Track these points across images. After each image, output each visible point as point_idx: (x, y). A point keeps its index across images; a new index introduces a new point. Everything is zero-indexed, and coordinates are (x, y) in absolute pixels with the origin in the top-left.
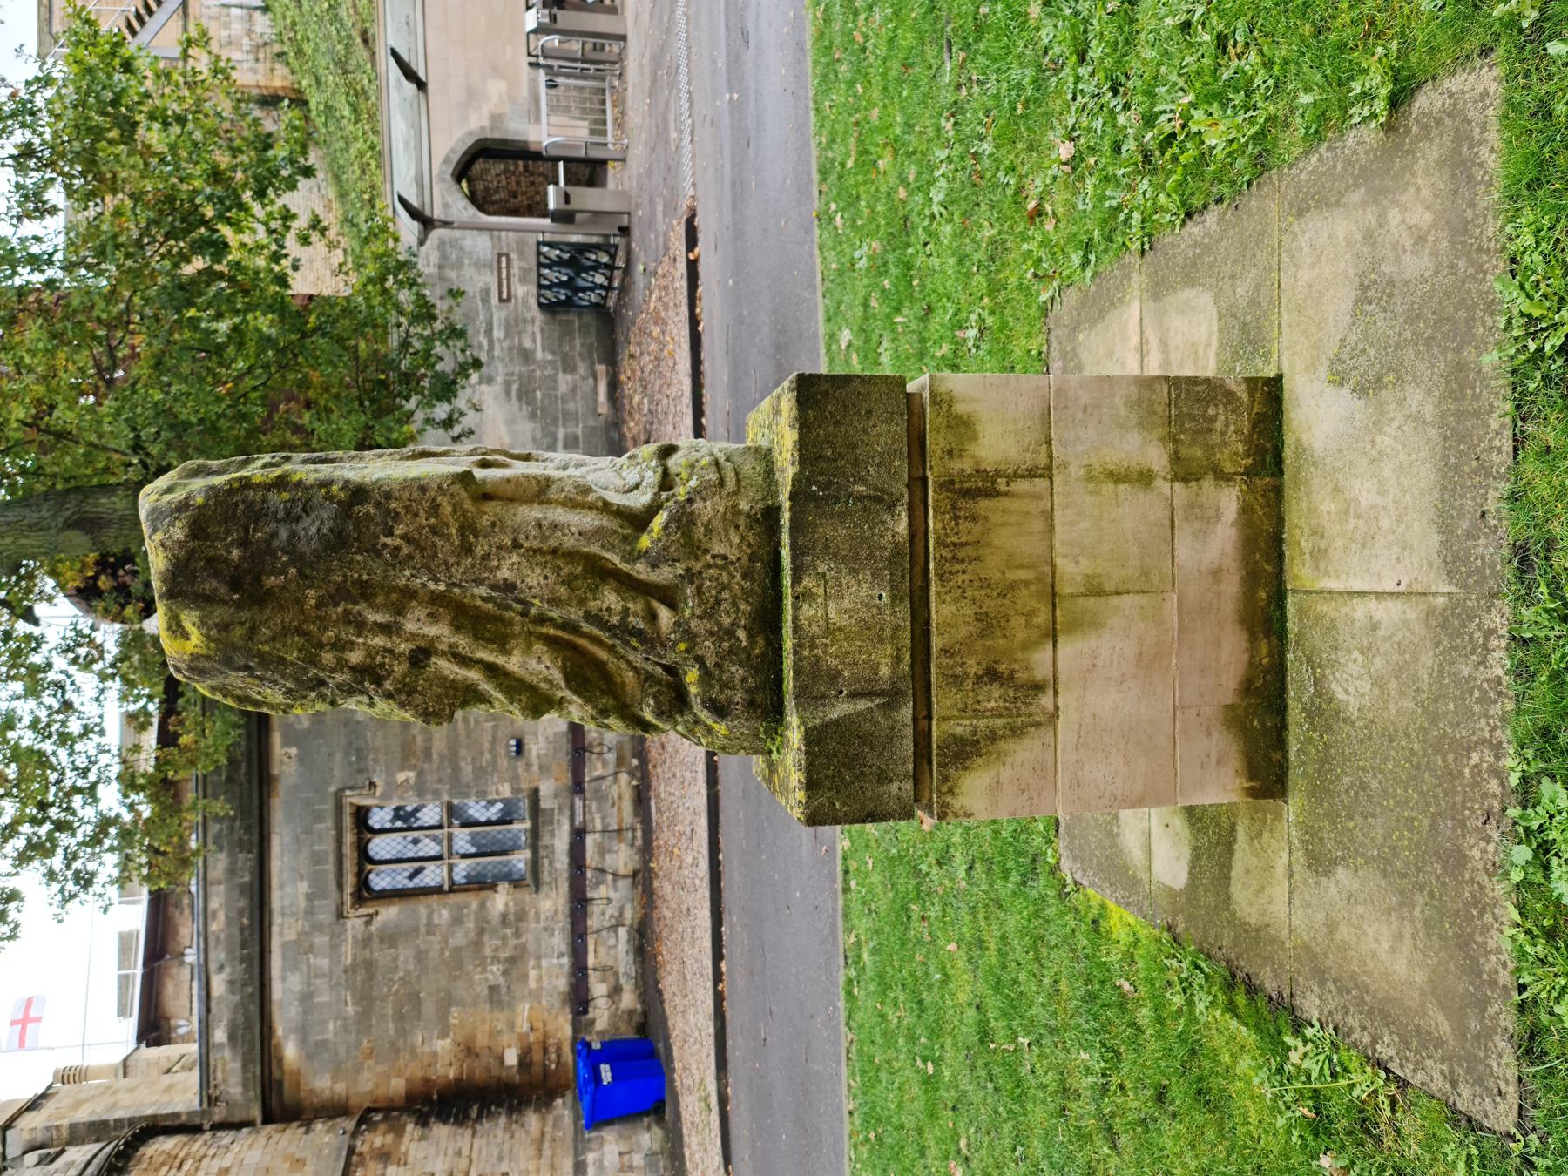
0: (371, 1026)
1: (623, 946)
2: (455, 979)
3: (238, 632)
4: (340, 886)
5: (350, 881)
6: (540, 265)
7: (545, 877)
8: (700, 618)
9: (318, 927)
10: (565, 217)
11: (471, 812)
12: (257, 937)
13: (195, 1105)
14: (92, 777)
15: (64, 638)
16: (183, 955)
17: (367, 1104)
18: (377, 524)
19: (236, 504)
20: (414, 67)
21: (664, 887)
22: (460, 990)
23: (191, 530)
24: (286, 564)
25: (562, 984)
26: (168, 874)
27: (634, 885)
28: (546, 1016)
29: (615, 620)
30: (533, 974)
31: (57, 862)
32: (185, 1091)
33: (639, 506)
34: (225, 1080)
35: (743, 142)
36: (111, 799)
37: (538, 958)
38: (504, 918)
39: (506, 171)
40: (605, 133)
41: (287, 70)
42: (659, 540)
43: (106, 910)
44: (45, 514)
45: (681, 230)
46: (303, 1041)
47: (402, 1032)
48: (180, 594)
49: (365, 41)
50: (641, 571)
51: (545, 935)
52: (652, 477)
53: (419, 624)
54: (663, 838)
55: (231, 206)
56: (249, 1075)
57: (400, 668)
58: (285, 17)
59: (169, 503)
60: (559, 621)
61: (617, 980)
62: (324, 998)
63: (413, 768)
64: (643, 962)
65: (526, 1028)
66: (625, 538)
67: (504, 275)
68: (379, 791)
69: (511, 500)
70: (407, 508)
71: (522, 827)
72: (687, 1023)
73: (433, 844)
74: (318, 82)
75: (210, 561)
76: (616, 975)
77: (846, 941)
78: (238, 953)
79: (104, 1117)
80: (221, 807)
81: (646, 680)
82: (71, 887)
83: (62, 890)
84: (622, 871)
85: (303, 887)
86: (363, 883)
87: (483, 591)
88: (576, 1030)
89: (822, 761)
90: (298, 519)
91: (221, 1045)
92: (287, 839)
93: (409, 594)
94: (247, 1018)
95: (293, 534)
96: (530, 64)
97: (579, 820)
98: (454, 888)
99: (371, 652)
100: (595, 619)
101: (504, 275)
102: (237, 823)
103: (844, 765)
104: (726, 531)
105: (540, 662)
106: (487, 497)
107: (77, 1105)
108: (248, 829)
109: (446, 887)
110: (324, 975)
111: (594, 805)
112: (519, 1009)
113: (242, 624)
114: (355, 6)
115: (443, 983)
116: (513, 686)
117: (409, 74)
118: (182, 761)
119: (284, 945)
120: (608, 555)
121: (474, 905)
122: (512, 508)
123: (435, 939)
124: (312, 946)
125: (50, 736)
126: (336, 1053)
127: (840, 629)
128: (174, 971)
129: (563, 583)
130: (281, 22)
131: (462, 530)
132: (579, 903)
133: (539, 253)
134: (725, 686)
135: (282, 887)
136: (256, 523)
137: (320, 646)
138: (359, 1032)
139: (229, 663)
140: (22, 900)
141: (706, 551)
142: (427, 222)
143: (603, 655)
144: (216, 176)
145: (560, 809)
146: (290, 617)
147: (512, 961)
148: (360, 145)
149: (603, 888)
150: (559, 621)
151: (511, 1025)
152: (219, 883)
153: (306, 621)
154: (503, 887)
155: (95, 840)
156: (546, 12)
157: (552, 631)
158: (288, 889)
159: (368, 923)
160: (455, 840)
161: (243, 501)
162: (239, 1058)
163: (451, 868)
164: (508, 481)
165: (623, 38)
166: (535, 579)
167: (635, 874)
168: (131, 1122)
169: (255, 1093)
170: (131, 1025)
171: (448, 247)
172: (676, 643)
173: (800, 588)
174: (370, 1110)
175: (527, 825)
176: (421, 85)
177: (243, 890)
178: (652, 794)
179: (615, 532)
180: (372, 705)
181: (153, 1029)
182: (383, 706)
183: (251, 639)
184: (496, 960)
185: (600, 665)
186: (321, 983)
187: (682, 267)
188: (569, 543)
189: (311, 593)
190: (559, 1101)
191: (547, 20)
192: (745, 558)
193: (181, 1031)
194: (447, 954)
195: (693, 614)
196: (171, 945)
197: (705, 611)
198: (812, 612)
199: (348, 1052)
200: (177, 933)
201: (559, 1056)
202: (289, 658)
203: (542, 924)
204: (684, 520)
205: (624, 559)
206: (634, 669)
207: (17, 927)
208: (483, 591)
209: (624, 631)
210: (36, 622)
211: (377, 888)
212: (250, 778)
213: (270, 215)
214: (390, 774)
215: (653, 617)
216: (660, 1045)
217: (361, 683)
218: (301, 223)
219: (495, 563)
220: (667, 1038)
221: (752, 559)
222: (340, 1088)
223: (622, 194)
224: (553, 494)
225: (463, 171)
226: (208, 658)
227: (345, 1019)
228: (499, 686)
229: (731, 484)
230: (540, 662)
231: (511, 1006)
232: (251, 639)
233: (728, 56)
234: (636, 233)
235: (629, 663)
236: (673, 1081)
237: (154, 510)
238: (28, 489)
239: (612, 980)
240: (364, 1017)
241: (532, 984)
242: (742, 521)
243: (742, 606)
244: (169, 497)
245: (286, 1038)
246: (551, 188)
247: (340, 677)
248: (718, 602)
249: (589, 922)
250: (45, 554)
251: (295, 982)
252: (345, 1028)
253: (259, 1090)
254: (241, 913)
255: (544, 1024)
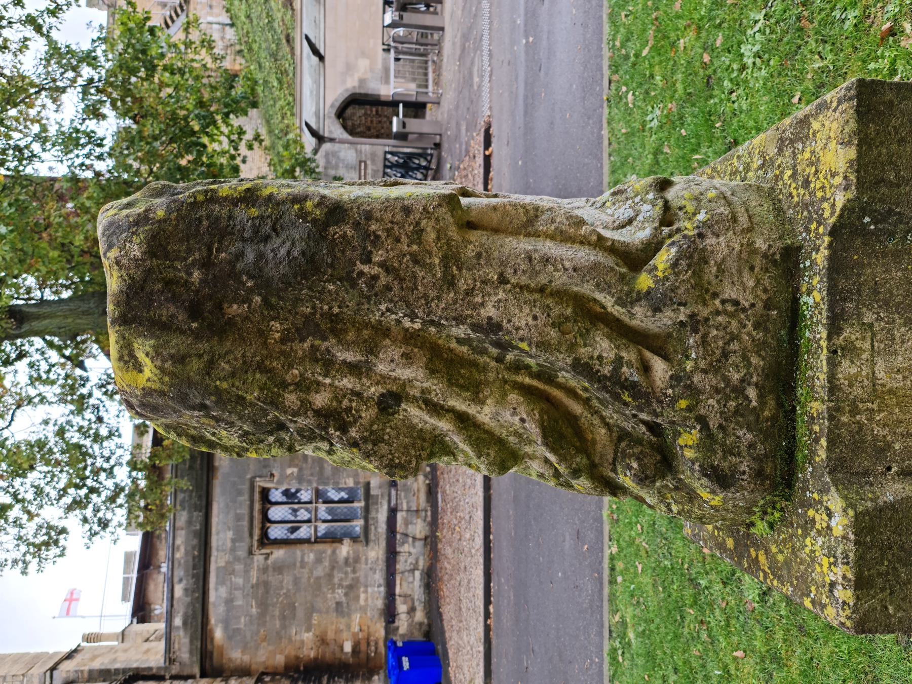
0: (266, 622)
1: (417, 583)
2: (316, 596)
3: (195, 365)
4: (251, 535)
5: (257, 532)
6: (385, 166)
7: (372, 536)
8: (705, 372)
9: (237, 559)
10: (402, 136)
11: (329, 494)
12: (202, 563)
13: (161, 662)
14: (112, 462)
15: (100, 379)
16: (160, 567)
17: (261, 669)
18: (354, 249)
19: (200, 220)
20: (317, 46)
21: (446, 550)
22: (319, 603)
23: (149, 246)
24: (250, 291)
25: (380, 603)
26: (152, 523)
27: (425, 545)
28: (369, 623)
29: (607, 370)
30: (362, 596)
31: (89, 512)
32: (156, 653)
33: (637, 242)
34: (179, 649)
35: (535, 65)
36: (122, 475)
37: (366, 586)
38: (347, 560)
39: (365, 114)
40: (426, 87)
41: (243, 62)
42: (666, 279)
43: (115, 542)
44: (92, 305)
45: (481, 138)
46: (226, 628)
47: (284, 627)
48: (134, 320)
49: (288, 41)
50: (640, 317)
51: (371, 573)
52: (649, 210)
53: (392, 366)
54: (446, 518)
55: (209, 121)
56: (194, 647)
57: (368, 414)
58: (243, 29)
59: (127, 216)
60: (535, 369)
61: (413, 603)
62: (239, 602)
63: (296, 466)
64: (429, 593)
65: (357, 629)
66: (622, 277)
67: (363, 174)
68: (275, 480)
69: (496, 231)
70: (388, 231)
71: (359, 505)
72: (462, 639)
73: (306, 513)
74: (260, 66)
75: (168, 283)
76: (413, 600)
77: (609, 619)
78: (191, 572)
79: (109, 667)
80: (185, 484)
81: (620, 439)
82: (96, 528)
83: (91, 529)
84: (418, 536)
85: (230, 534)
86: (264, 534)
87: (461, 331)
88: (387, 632)
89: (875, 553)
90: (266, 239)
91: (178, 628)
92: (222, 505)
93: (382, 331)
94: (194, 612)
95: (261, 256)
96: (384, 50)
97: (393, 503)
98: (318, 540)
99: (338, 395)
100: (582, 368)
101: (363, 174)
102: (194, 494)
103: (900, 561)
104: (740, 272)
105: (514, 413)
106: (471, 225)
107: (94, 658)
108: (200, 497)
109: (313, 540)
110: (240, 589)
111: (403, 494)
112: (353, 617)
113: (200, 356)
114: (283, 20)
115: (309, 598)
116: (484, 439)
117: (315, 51)
118: (164, 455)
119: (218, 569)
120: (599, 296)
121: (329, 552)
122: (499, 239)
123: (306, 571)
124: (234, 570)
125: (89, 436)
126: (245, 637)
127: (891, 392)
128: (155, 576)
129: (553, 325)
130: (240, 32)
131: (445, 259)
132: (392, 554)
133: (385, 159)
134: (729, 451)
135: (218, 534)
136: (220, 242)
137: (284, 385)
138: (259, 625)
139: (183, 400)
140: (67, 533)
141: (715, 295)
142: (320, 139)
143: (577, 408)
144: (201, 104)
145: (382, 495)
146: (253, 351)
147: (351, 587)
148: (282, 103)
149: (406, 546)
150: (535, 369)
151: (349, 627)
152: (182, 529)
153: (270, 356)
154: (346, 541)
155: (112, 499)
156: (397, 13)
157: (527, 380)
158: (221, 535)
159: (266, 559)
160: (319, 511)
161: (208, 217)
162: (188, 636)
163: (316, 528)
164: (495, 208)
165: (442, 29)
166: (522, 318)
167: (426, 538)
168: (124, 671)
169: (196, 658)
170: (128, 607)
171: (331, 157)
172: (674, 400)
173: (840, 341)
174: (263, 674)
175: (362, 504)
176: (321, 58)
177: (196, 534)
178: (439, 490)
179: (612, 269)
180: (330, 452)
181: (141, 612)
182: (343, 453)
183: (208, 374)
184: (340, 586)
185: (572, 419)
186: (238, 594)
187: (480, 160)
188: (560, 280)
189: (276, 325)
190: (376, 678)
191: (397, 18)
192: (760, 305)
193: (157, 612)
194: (312, 580)
195: (696, 368)
196: (154, 561)
197: (711, 364)
198: (854, 370)
199: (252, 637)
200: (157, 554)
201: (376, 648)
202: (248, 397)
203: (369, 566)
204: (694, 257)
205: (620, 302)
206: (607, 425)
207: (64, 549)
208: (461, 331)
209: (613, 384)
210: (85, 369)
211: (272, 537)
212: (202, 469)
213: (231, 132)
214: (283, 469)
215: (646, 369)
216: (439, 647)
217: (325, 429)
218: (249, 136)
219: (479, 299)
220: (444, 644)
221: (767, 306)
222: (246, 658)
223: (437, 123)
224: (541, 226)
225: (341, 113)
226: (161, 393)
227: (251, 616)
228: (469, 439)
229: (743, 220)
230: (514, 413)
231: (349, 615)
232: (208, 374)
233: (526, 14)
234: (445, 146)
235: (603, 418)
236: (447, 672)
237: (111, 224)
238: (85, 292)
239: (410, 603)
240: (262, 614)
241: (362, 602)
242: (758, 262)
243: (754, 360)
244: (125, 212)
245: (216, 625)
246: (395, 119)
247: (302, 421)
248: (725, 355)
249: (398, 567)
250: (91, 329)
251: (223, 591)
252: (251, 622)
253: (199, 656)
254: (194, 548)
255: (368, 627)
